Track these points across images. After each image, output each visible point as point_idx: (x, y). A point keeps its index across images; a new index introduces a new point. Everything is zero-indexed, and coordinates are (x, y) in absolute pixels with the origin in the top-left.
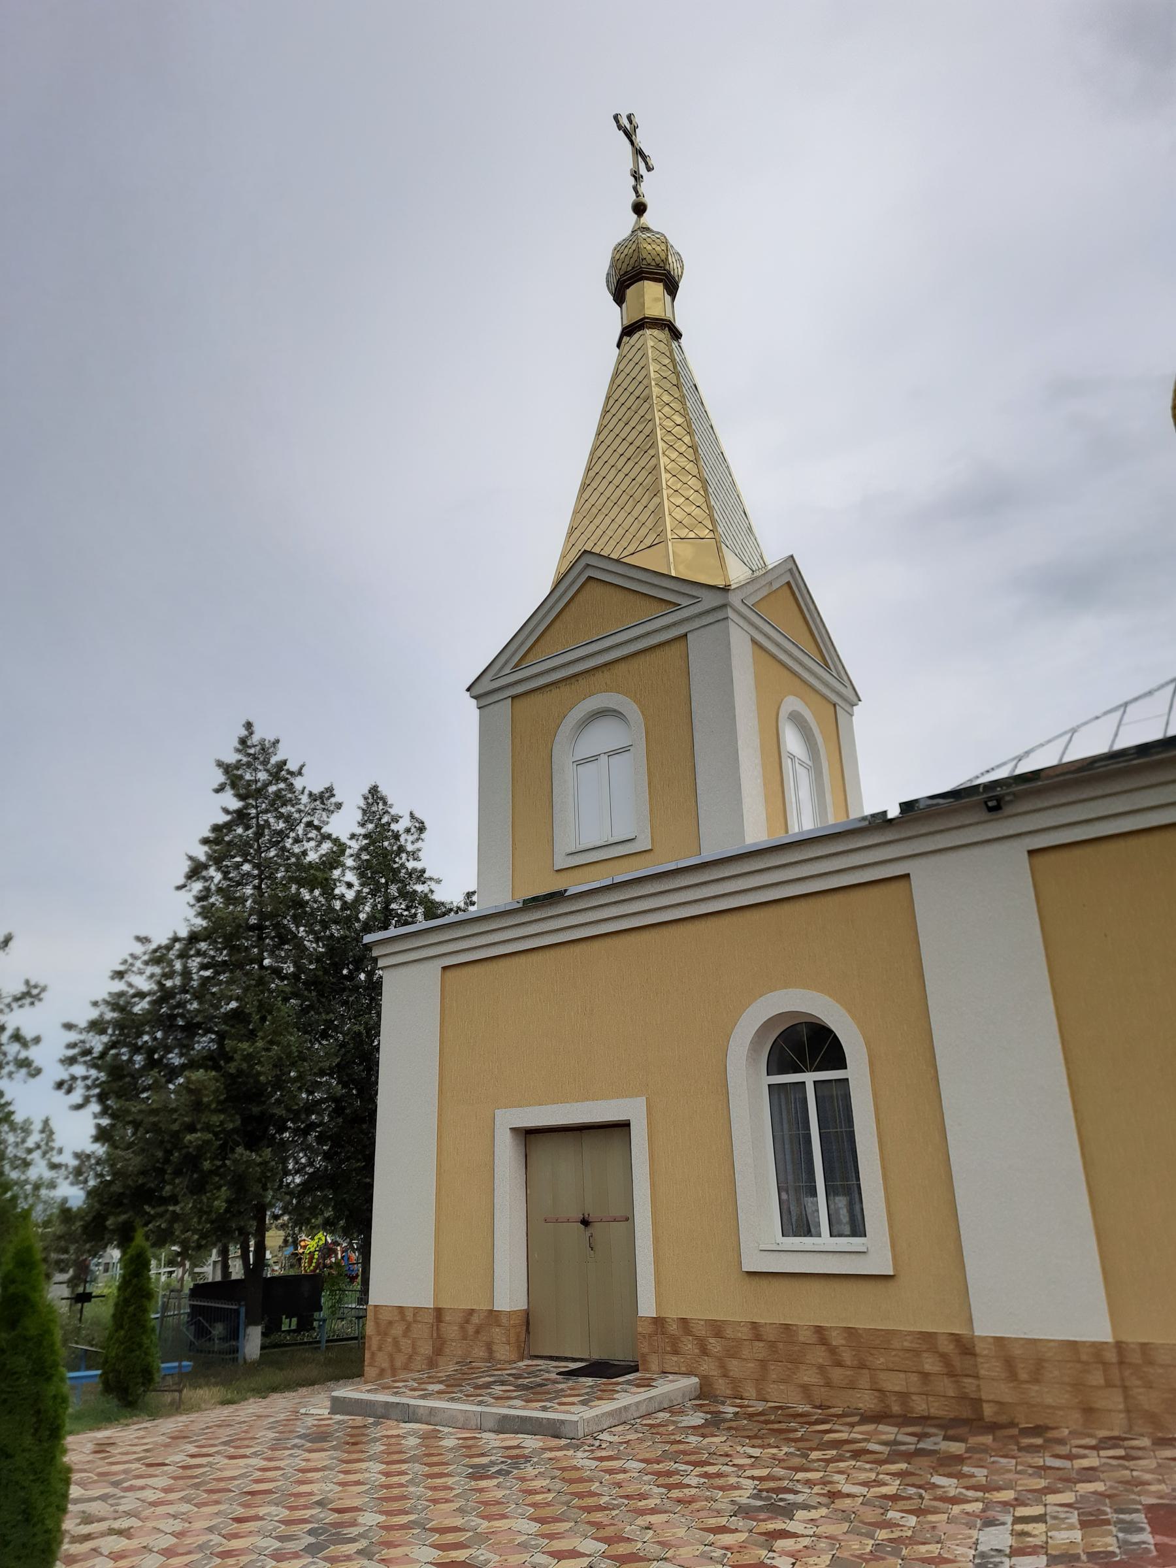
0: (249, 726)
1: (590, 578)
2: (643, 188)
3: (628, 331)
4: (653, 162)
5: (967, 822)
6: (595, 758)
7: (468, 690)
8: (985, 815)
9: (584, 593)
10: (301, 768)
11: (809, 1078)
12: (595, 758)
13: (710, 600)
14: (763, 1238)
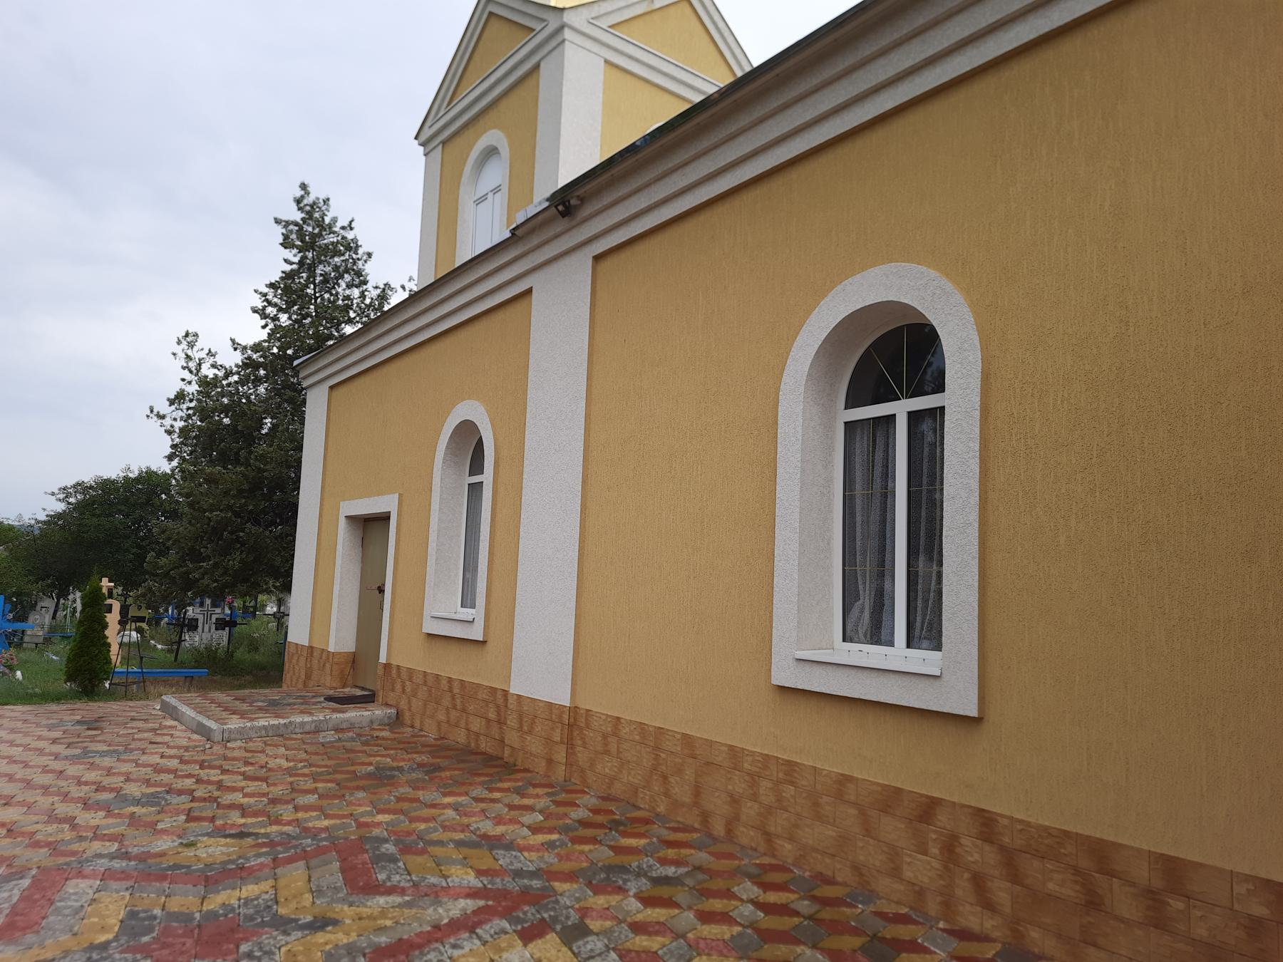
1: (491, 14)
6: (483, 198)
7: (416, 138)
8: (561, 224)
11: (900, 409)
12: (483, 198)
14: (808, 635)
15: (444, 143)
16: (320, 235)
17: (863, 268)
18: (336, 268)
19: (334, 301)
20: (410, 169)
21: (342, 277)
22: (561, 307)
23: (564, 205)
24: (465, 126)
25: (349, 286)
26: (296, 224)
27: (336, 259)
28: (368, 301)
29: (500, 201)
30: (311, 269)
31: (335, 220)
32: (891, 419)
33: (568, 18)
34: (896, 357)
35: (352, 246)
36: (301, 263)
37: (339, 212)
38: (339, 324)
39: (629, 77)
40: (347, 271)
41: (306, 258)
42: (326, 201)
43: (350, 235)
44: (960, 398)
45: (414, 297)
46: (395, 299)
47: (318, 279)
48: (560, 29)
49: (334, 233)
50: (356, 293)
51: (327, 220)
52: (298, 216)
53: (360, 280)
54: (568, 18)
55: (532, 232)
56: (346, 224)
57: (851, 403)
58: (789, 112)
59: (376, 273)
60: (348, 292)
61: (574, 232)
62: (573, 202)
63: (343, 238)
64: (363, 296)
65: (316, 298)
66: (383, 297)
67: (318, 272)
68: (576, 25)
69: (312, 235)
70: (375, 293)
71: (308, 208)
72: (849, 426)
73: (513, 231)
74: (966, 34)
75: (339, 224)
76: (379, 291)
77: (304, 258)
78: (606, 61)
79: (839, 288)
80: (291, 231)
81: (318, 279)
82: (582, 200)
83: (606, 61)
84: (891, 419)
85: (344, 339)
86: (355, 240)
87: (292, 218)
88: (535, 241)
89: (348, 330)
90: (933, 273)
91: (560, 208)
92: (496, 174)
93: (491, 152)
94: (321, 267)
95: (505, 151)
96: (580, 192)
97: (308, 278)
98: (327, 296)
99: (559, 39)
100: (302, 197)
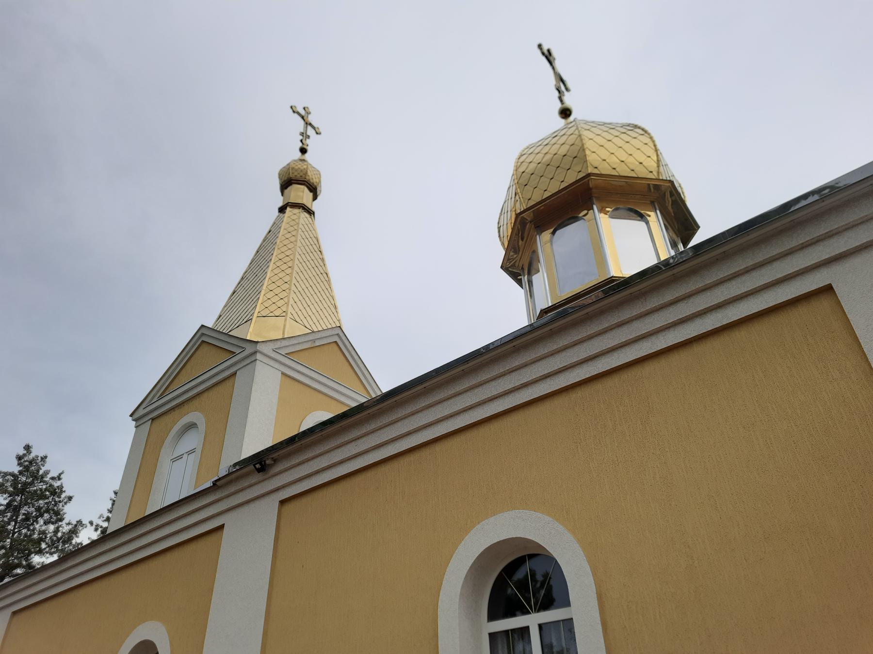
0: (28, 448)
1: (203, 342)
2: (565, 99)
3: (282, 210)
4: (569, 84)
5: (253, 481)
6: (180, 457)
7: (131, 415)
8: (258, 477)
9: (199, 352)
10: (60, 474)
11: (532, 621)
12: (180, 457)
13: (249, 349)
15: (153, 419)
16: (32, 483)
17: (494, 514)
18: (38, 509)
19: (31, 535)
20: (121, 439)
21: (42, 516)
22: (249, 539)
23: (261, 464)
24: (173, 409)
25: (46, 523)
26: (12, 475)
27: (41, 502)
28: (60, 535)
29: (192, 461)
30: (16, 510)
31: (47, 473)
32: (524, 632)
33: (259, 347)
34: (520, 583)
35: (56, 492)
36: (9, 505)
37: (51, 468)
38: (29, 555)
39: (296, 383)
40: (47, 511)
41: (15, 500)
42: (44, 459)
43: (56, 484)
44: (582, 607)
45: (105, 536)
46: (86, 536)
47: (21, 517)
48: (255, 353)
49: (44, 482)
50: (52, 528)
51: (41, 472)
52: (16, 469)
53: (58, 517)
54: (259, 347)
55: (230, 483)
56: (56, 475)
57: (493, 616)
58: (433, 409)
59: (71, 513)
60: (44, 528)
61: (266, 482)
62: (268, 462)
63: (51, 485)
64: (56, 531)
65: (14, 533)
66: (74, 531)
67: (23, 511)
68: (265, 352)
69: (25, 484)
70: (66, 529)
71: (27, 463)
72: (493, 636)
73: (215, 483)
74: (546, 372)
75: (49, 476)
76: (70, 527)
77: (11, 501)
78: (283, 374)
79: (479, 526)
80: (7, 481)
81: (21, 517)
82: (275, 461)
83: (283, 374)
84: (524, 632)
85: (31, 570)
86: (61, 488)
87: (10, 470)
88: (232, 489)
89: (37, 560)
90: (547, 518)
91: (258, 466)
92: (192, 440)
93: (192, 426)
94: (26, 508)
95: (202, 426)
96: (275, 455)
97: (12, 516)
98: (24, 531)
99: (253, 359)
100: (24, 455)
